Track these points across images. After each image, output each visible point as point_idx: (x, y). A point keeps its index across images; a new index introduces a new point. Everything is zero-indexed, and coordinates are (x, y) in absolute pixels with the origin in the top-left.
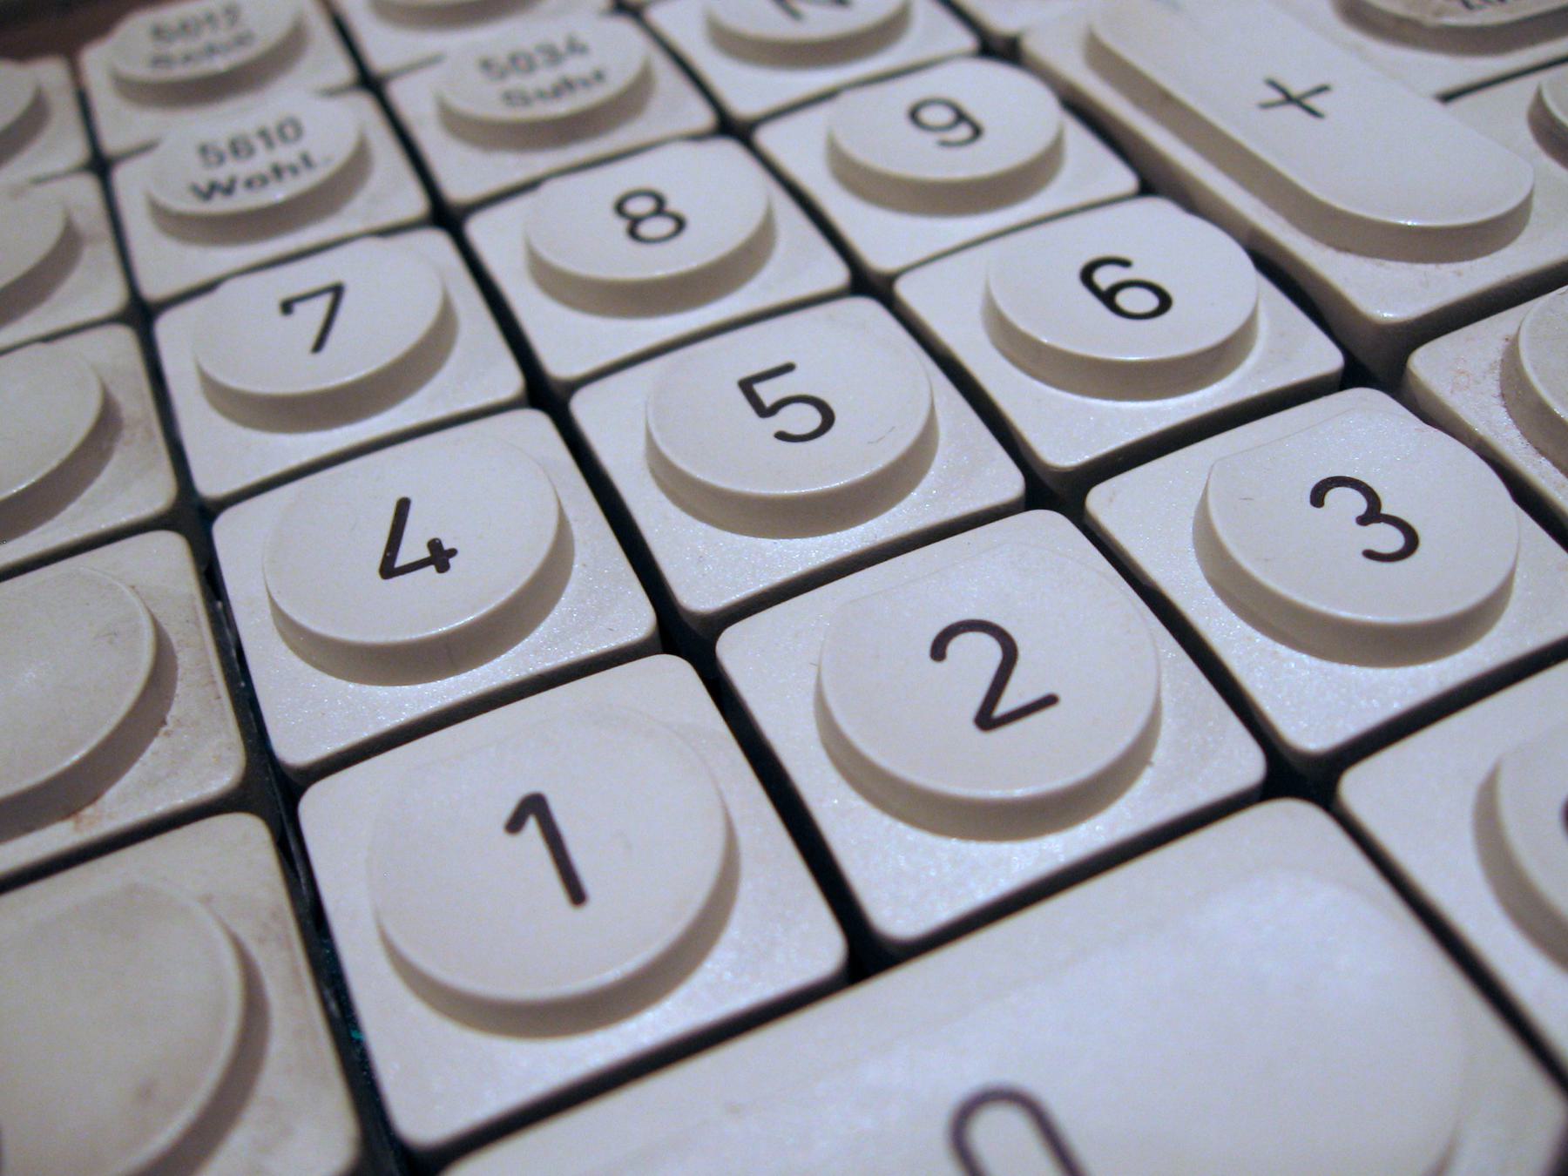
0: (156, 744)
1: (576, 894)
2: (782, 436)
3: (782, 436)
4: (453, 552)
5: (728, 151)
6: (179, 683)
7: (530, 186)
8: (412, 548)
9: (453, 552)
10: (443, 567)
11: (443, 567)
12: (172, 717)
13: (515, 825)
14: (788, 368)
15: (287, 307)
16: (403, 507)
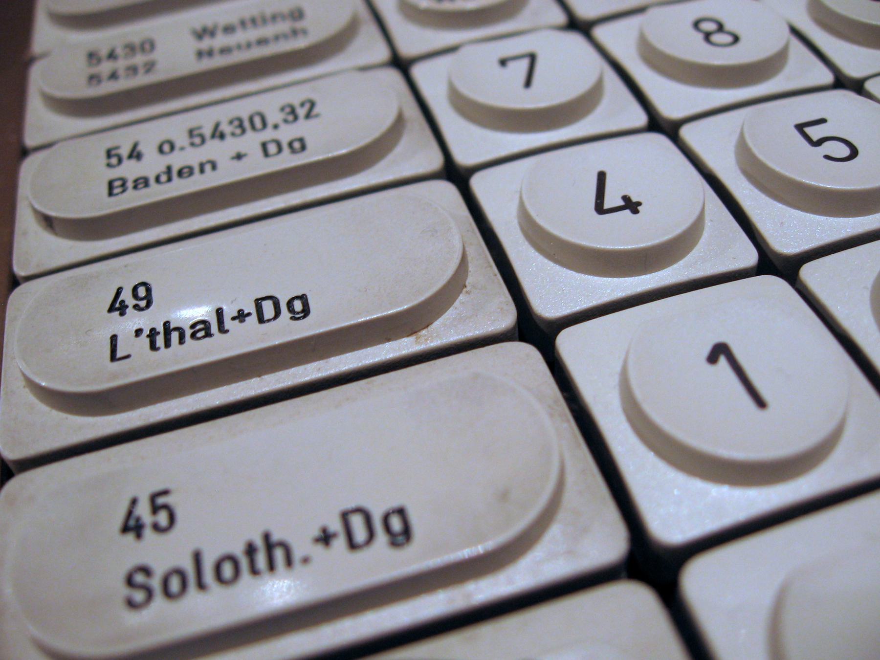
0: (462, 297)
1: (761, 403)
2: (827, 157)
3: (827, 157)
4: (639, 204)
5: (575, 40)
6: (470, 265)
7: (451, 50)
8: (612, 199)
9: (639, 204)
10: (635, 211)
11: (635, 211)
12: (469, 283)
13: (712, 358)
14: (823, 121)
15: (503, 62)
16: (602, 177)
